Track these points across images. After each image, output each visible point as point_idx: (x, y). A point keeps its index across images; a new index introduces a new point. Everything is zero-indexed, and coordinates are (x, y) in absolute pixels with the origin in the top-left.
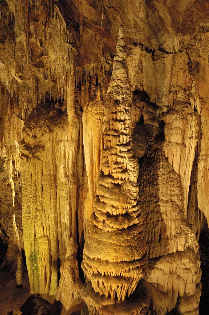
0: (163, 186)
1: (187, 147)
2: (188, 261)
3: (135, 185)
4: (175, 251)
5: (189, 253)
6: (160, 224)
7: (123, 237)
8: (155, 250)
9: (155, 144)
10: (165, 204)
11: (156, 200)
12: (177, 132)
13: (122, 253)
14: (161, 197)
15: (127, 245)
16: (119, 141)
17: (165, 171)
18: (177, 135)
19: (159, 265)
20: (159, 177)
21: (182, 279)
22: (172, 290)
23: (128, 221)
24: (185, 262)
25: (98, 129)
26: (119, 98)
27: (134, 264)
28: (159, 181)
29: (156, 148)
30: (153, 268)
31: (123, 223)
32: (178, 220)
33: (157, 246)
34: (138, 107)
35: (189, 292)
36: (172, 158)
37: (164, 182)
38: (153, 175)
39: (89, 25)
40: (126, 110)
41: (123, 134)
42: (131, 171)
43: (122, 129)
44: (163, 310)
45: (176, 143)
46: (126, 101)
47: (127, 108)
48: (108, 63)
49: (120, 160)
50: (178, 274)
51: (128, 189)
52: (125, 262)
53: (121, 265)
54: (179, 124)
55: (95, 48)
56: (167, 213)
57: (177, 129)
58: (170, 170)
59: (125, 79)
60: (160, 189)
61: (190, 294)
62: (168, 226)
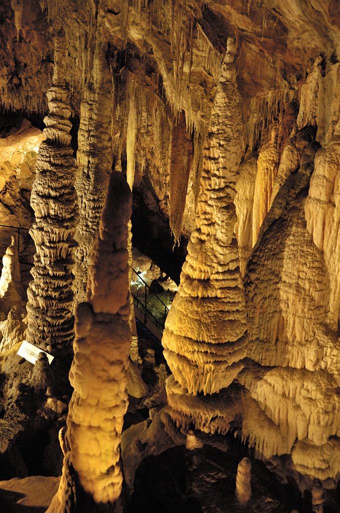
0: (288, 261)
1: (337, 207)
2: (314, 388)
3: (222, 244)
4: (298, 366)
5: (319, 376)
6: (277, 315)
7: (192, 306)
8: (269, 354)
9: (293, 200)
10: (286, 289)
11: (276, 280)
12: (319, 182)
13: (187, 326)
14: (284, 278)
15: (195, 318)
16: (210, 185)
17: (296, 241)
18: (318, 187)
19: (268, 377)
20: (286, 248)
21: (301, 412)
22: (285, 422)
23: (203, 288)
24: (309, 388)
25: (263, 182)
26: (214, 129)
27: (200, 346)
28: (285, 253)
29: (293, 207)
30: (261, 379)
31: (196, 289)
32: (308, 318)
33: (271, 350)
34: (297, 148)
35: (313, 438)
36: (311, 222)
37: (291, 256)
38: (281, 243)
39: (250, 38)
40: (220, 145)
41: (215, 175)
42: (218, 225)
43: (214, 170)
44: (267, 447)
45: (317, 200)
46: (222, 133)
47: (222, 143)
48: (294, 89)
49: (208, 209)
50: (298, 404)
51: (212, 247)
52: (190, 339)
53: (184, 340)
54: (323, 170)
55: (267, 69)
56: (289, 302)
57: (318, 178)
58: (304, 240)
59: (225, 105)
60: (284, 264)
61: (314, 442)
62: (288, 323)
